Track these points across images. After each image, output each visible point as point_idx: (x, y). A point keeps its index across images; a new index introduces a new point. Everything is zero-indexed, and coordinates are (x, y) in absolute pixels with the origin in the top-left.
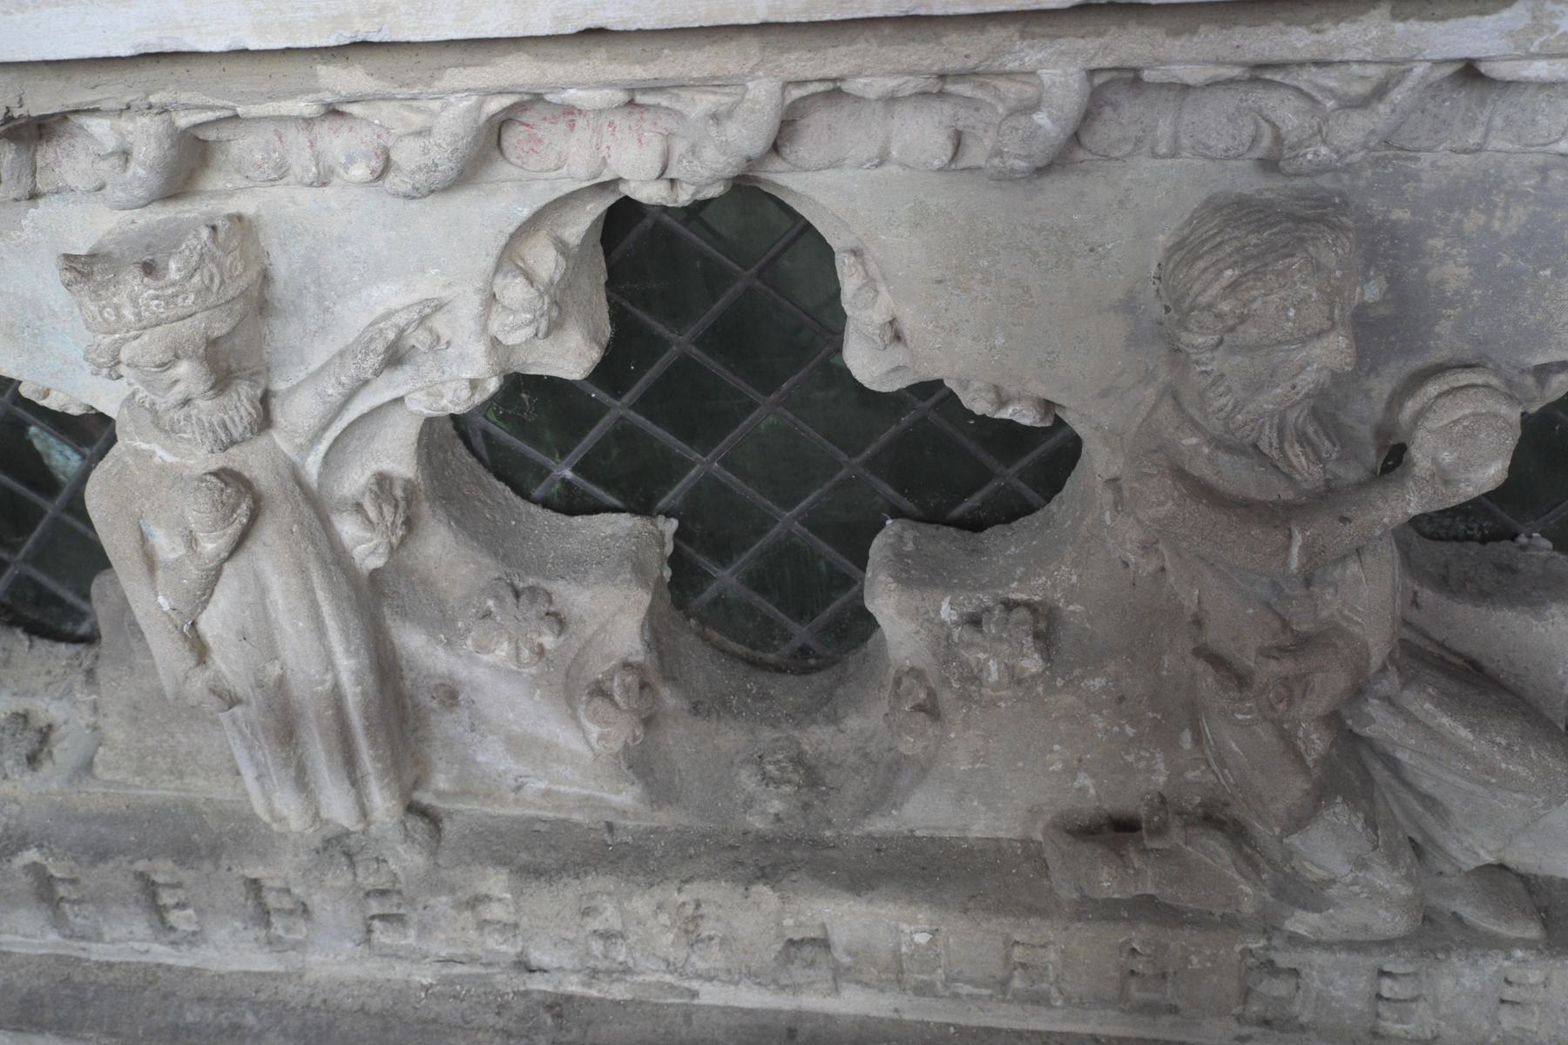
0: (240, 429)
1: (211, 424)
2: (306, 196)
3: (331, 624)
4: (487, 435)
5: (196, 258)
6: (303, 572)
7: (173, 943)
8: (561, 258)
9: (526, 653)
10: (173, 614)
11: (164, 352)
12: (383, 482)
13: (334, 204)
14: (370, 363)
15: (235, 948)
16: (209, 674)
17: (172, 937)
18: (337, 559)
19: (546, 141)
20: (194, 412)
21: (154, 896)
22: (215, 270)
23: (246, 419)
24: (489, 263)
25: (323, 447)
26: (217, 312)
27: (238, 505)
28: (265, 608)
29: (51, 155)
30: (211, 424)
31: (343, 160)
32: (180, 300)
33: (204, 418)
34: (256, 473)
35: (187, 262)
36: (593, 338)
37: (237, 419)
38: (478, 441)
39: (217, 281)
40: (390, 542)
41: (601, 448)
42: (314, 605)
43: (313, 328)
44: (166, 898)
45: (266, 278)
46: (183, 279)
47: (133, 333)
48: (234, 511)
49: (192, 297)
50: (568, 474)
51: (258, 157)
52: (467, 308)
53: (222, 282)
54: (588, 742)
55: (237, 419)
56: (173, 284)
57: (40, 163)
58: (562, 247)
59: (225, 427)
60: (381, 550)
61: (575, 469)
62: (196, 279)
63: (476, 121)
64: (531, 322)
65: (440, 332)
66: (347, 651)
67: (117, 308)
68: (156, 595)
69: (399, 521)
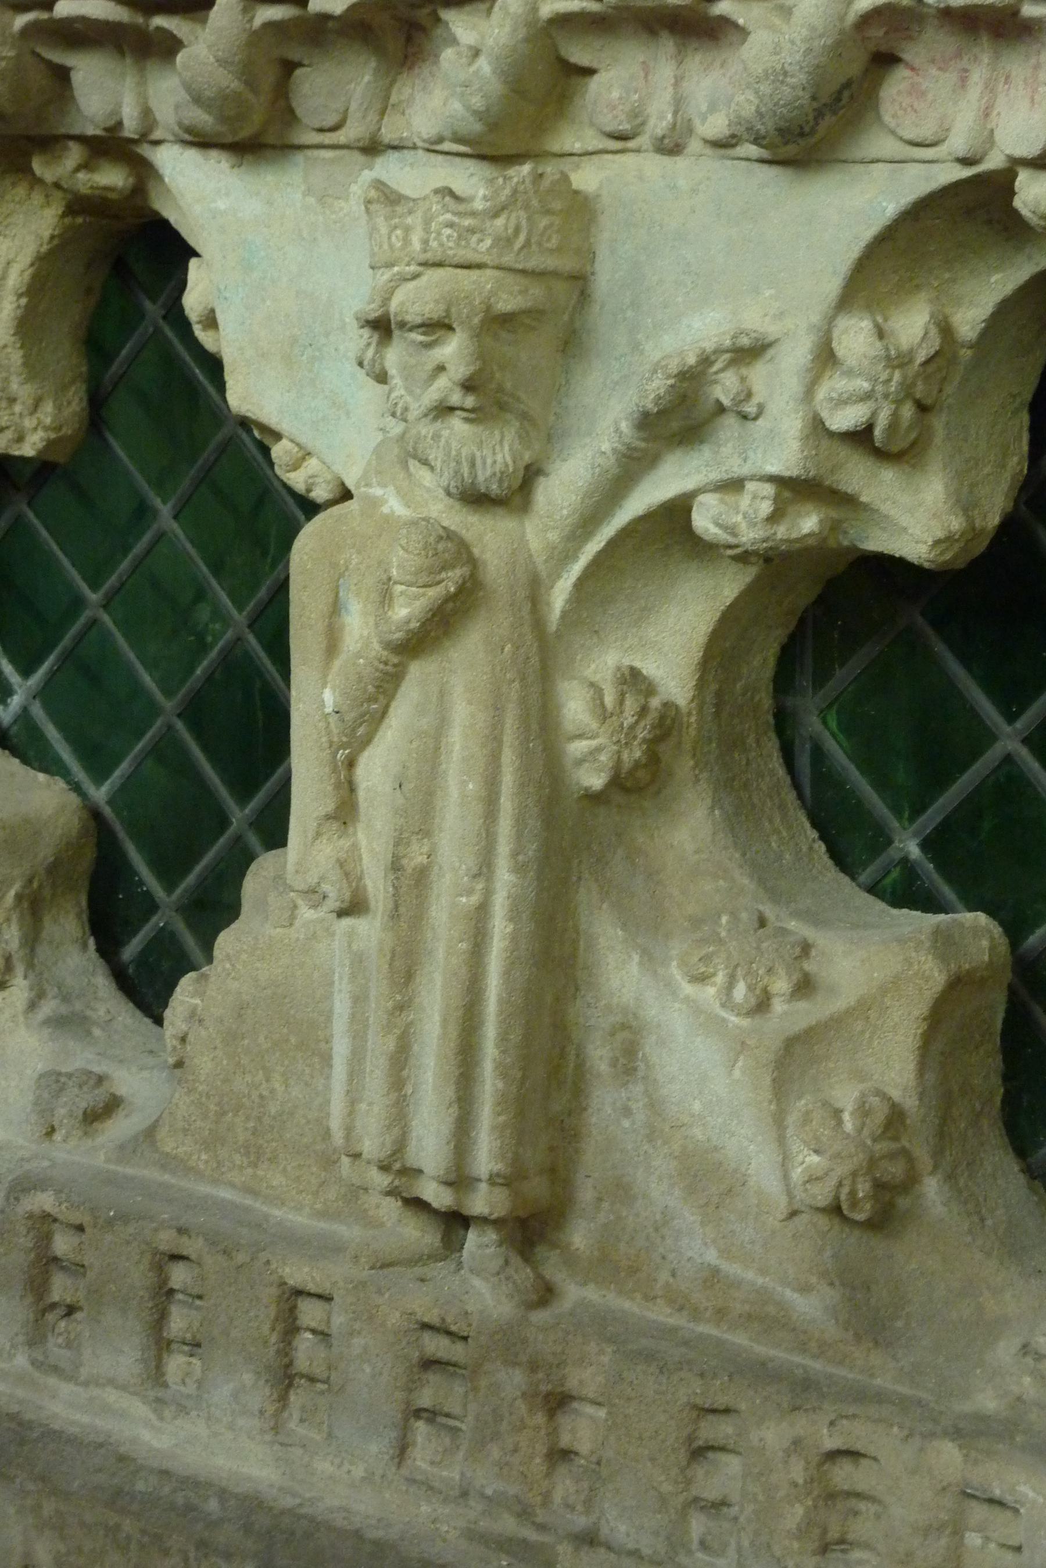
0: (488, 473)
1: (459, 454)
2: (654, 165)
3: (507, 805)
4: (818, 754)
5: (507, 191)
6: (497, 709)
7: (158, 1400)
8: (934, 332)
9: (740, 991)
10: (333, 720)
11: (437, 302)
12: (633, 680)
13: (682, 183)
14: (655, 384)
15: (231, 1427)
16: (345, 843)
17: (161, 1393)
18: (543, 728)
19: (930, 97)
20: (445, 433)
21: (162, 1317)
22: (524, 223)
23: (498, 468)
24: (832, 286)
25: (577, 568)
26: (509, 279)
27: (453, 567)
28: (437, 748)
29: (407, 91)
30: (459, 454)
31: (704, 108)
32: (474, 239)
33: (454, 445)
34: (487, 556)
35: (496, 193)
36: (966, 505)
37: (489, 461)
38: (804, 762)
39: (522, 238)
40: (619, 761)
41: (971, 809)
42: (495, 758)
43: (616, 377)
44: (178, 1322)
45: (580, 282)
46: (485, 212)
47: (413, 268)
48: (443, 568)
49: (488, 242)
50: (914, 850)
51: (615, 94)
52: (795, 355)
53: (527, 244)
54: (786, 1176)
55: (489, 461)
56: (473, 214)
57: (394, 99)
58: (946, 330)
59: (473, 465)
60: (603, 758)
61: (926, 845)
62: (500, 222)
63: (842, 18)
64: (867, 396)
65: (755, 389)
66: (515, 854)
67: (407, 230)
68: (324, 686)
69: (642, 734)
